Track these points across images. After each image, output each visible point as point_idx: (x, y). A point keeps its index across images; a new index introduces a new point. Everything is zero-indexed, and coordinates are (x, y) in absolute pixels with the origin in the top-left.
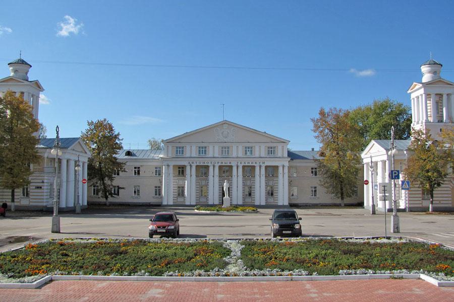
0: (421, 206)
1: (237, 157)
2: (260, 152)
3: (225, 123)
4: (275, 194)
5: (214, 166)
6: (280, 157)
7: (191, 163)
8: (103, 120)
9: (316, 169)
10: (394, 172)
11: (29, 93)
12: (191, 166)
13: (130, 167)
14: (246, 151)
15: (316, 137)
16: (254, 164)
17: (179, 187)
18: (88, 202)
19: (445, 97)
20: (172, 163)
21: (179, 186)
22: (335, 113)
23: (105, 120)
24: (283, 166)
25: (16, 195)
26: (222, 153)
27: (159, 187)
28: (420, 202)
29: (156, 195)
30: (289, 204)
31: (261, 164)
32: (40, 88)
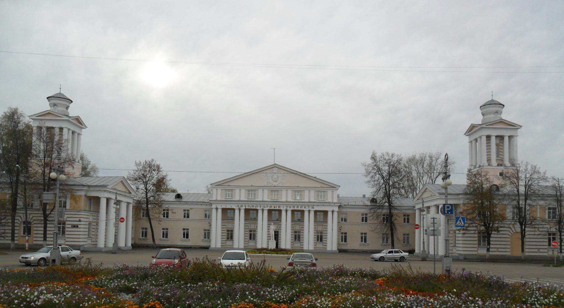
0: (476, 253)
3: (275, 166)
4: (324, 239)
5: (240, 210)
6: (329, 202)
7: (240, 206)
8: (150, 160)
9: (366, 215)
10: (446, 206)
11: (69, 129)
12: (240, 210)
13: (178, 210)
15: (369, 182)
18: (132, 245)
19: (506, 139)
22: (387, 158)
23: (153, 160)
24: (333, 212)
27: (208, 230)
28: (476, 249)
29: (205, 238)
32: (81, 124)
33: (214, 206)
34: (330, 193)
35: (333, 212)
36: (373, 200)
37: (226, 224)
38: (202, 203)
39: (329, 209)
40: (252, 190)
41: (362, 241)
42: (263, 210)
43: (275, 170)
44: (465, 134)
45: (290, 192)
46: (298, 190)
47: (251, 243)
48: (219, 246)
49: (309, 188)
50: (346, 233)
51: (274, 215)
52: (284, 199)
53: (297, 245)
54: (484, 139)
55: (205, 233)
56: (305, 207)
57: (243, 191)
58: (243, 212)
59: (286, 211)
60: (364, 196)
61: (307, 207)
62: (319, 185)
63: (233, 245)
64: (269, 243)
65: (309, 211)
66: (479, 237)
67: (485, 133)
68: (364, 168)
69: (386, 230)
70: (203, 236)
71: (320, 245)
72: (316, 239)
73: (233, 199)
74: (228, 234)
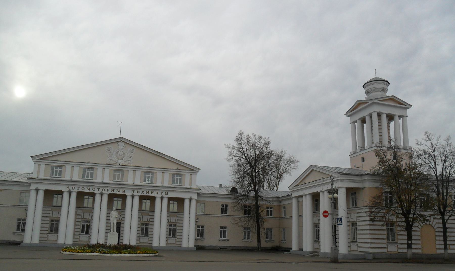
0: (385, 250)
1: (134, 185)
2: (103, 177)
3: (121, 140)
5: (70, 193)
6: (186, 188)
7: (70, 188)
12: (70, 193)
14: (145, 177)
16: (154, 195)
17: (52, 221)
20: (43, 187)
21: (53, 219)
24: (190, 200)
25: (449, 232)
26: (145, 181)
30: (195, 246)
31: (164, 195)
33: (33, 186)
34: (187, 177)
35: (190, 200)
36: (234, 190)
37: (50, 212)
38: (20, 183)
39: (186, 196)
40: (89, 169)
41: (221, 236)
42: (102, 194)
43: (121, 145)
44: (346, 114)
45: (138, 173)
46: (149, 172)
47: (84, 238)
48: (36, 240)
49: (163, 170)
50: (202, 227)
51: (116, 199)
52: (130, 182)
53: (144, 241)
54: (375, 116)
55: (19, 223)
56: (157, 193)
57: (77, 169)
58: (74, 196)
59: (133, 197)
60: (221, 186)
61: (159, 193)
62: (175, 167)
63: (57, 240)
64: (108, 238)
65: (162, 198)
66: (388, 229)
67: (376, 109)
68: (227, 150)
69: (252, 224)
70: (16, 227)
71: (172, 241)
72: (168, 233)
73: (62, 179)
74: (52, 225)
